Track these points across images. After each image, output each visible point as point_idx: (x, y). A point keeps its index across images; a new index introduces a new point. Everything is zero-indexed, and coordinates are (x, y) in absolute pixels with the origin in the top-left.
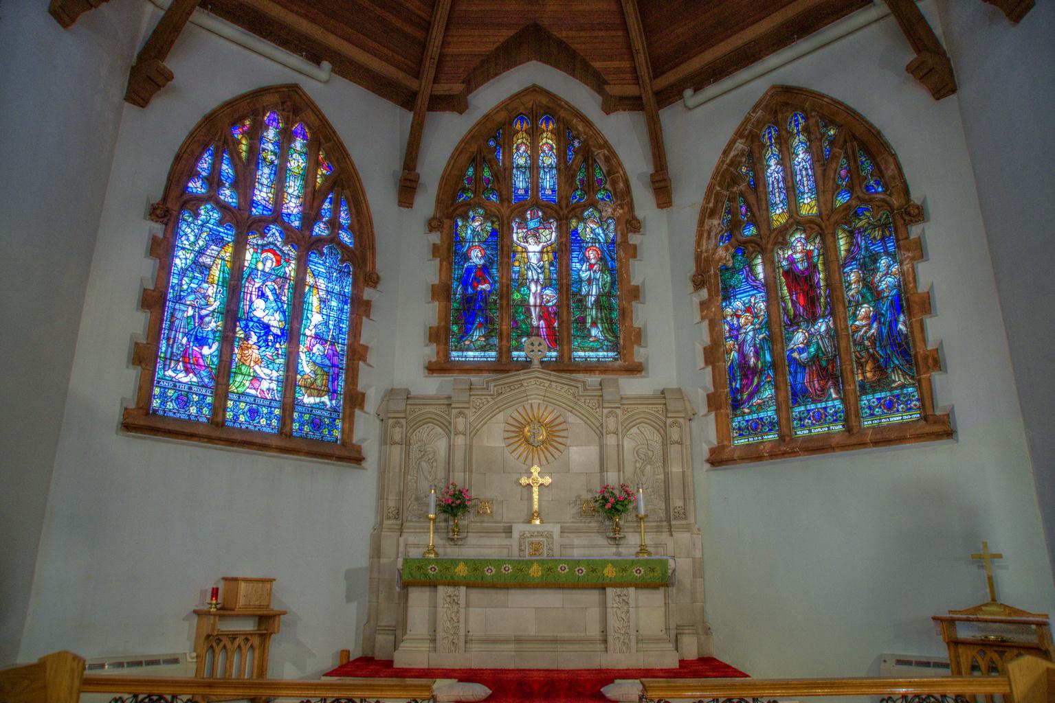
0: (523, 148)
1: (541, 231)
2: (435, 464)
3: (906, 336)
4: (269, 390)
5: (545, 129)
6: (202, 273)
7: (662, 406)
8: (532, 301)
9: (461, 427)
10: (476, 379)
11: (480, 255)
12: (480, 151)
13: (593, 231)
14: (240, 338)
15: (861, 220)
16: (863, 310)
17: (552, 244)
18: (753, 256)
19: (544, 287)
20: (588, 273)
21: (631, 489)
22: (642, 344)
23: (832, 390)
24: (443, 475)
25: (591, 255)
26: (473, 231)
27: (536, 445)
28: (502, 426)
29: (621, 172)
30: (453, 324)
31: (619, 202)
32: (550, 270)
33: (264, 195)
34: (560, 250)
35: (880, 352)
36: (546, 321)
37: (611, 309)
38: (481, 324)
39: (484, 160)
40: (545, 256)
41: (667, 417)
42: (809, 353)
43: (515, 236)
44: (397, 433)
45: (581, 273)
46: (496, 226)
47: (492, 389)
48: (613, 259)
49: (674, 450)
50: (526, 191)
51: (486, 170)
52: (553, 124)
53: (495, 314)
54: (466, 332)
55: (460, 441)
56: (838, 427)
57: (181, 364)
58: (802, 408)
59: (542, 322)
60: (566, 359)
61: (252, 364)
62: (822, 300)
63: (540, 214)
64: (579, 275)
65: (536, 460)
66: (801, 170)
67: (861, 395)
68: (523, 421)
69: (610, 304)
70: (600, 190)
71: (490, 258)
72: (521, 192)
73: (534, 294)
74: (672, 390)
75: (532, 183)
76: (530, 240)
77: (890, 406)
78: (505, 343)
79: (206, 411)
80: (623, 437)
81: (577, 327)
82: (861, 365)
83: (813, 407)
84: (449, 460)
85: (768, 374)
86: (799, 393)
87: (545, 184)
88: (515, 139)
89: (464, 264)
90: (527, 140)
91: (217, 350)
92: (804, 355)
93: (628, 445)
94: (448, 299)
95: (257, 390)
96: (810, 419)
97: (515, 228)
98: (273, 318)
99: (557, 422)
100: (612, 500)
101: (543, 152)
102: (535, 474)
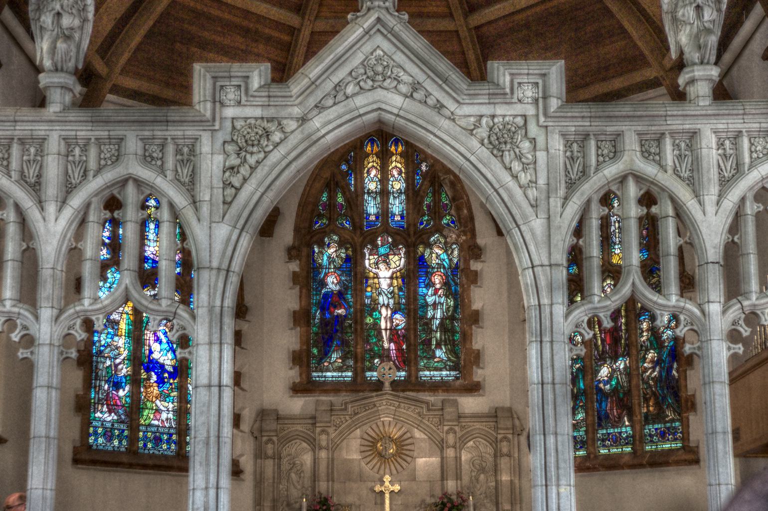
0: (373, 172)
1: (391, 257)
2: (302, 475)
3: (677, 381)
4: (167, 419)
5: (394, 152)
6: (113, 328)
7: (494, 423)
8: (383, 325)
9: (324, 443)
10: (337, 399)
11: (336, 282)
12: (333, 175)
13: (438, 256)
14: (144, 379)
15: (654, 277)
16: (650, 355)
17: (401, 270)
18: (575, 293)
19: (395, 312)
20: (434, 297)
21: (465, 496)
22: (481, 365)
23: (626, 419)
24: (310, 484)
25: (437, 280)
26: (329, 257)
27: (387, 457)
28: (359, 441)
29: (465, 198)
30: (313, 347)
31: (462, 229)
32: (399, 295)
33: (152, 249)
34: (408, 276)
35: (660, 392)
36: (395, 343)
37: (453, 332)
38: (337, 346)
39: (337, 184)
40: (395, 282)
41: (497, 433)
42: (611, 385)
43: (367, 262)
44: (270, 449)
45: (427, 297)
46: (350, 252)
47: (350, 410)
48: (456, 284)
49: (504, 463)
50: (377, 218)
51: (340, 195)
52: (402, 146)
53: (350, 337)
54: (325, 354)
55: (323, 454)
56: (628, 449)
57: (105, 406)
58: (605, 431)
59: (392, 346)
60: (413, 379)
61: (154, 400)
62: (623, 341)
63: (390, 240)
64: (425, 300)
65: (387, 470)
66: (615, 222)
67: (645, 425)
68: (376, 437)
69: (453, 326)
70: (445, 216)
71: (344, 284)
72: (373, 218)
73: (385, 318)
74: (503, 409)
75: (382, 209)
76: (382, 266)
77: (663, 435)
78: (359, 364)
79: (124, 443)
80: (461, 450)
81: (423, 349)
82: (646, 400)
83: (612, 430)
84: (314, 466)
85: (581, 399)
86: (603, 417)
87: (394, 209)
88: (366, 163)
89: (321, 290)
90: (377, 163)
91: (129, 391)
92: (608, 387)
93: (465, 456)
94: (308, 324)
95: (158, 420)
96: (609, 441)
97: (367, 255)
98: (166, 358)
99: (405, 437)
100: (449, 505)
101: (393, 176)
102: (387, 484)
